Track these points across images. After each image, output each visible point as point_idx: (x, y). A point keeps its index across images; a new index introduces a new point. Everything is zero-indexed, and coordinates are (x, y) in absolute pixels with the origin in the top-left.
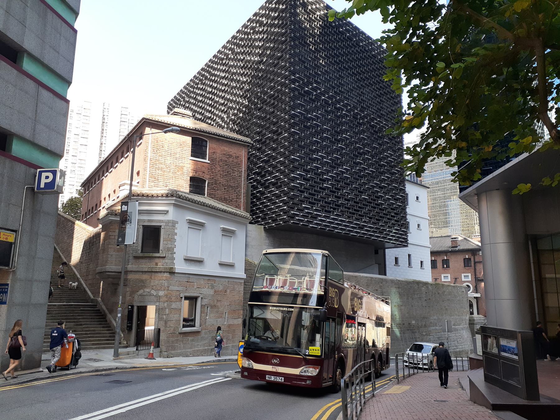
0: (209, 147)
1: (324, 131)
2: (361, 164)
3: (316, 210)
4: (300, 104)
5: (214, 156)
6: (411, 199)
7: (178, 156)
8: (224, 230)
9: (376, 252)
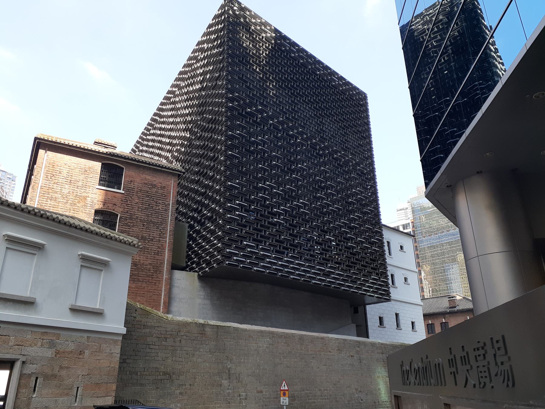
0: (127, 175)
1: (272, 158)
2: (323, 199)
3: (263, 249)
4: (239, 125)
5: (132, 185)
6: (395, 248)
7: (80, 184)
8: (84, 258)
9: (356, 311)
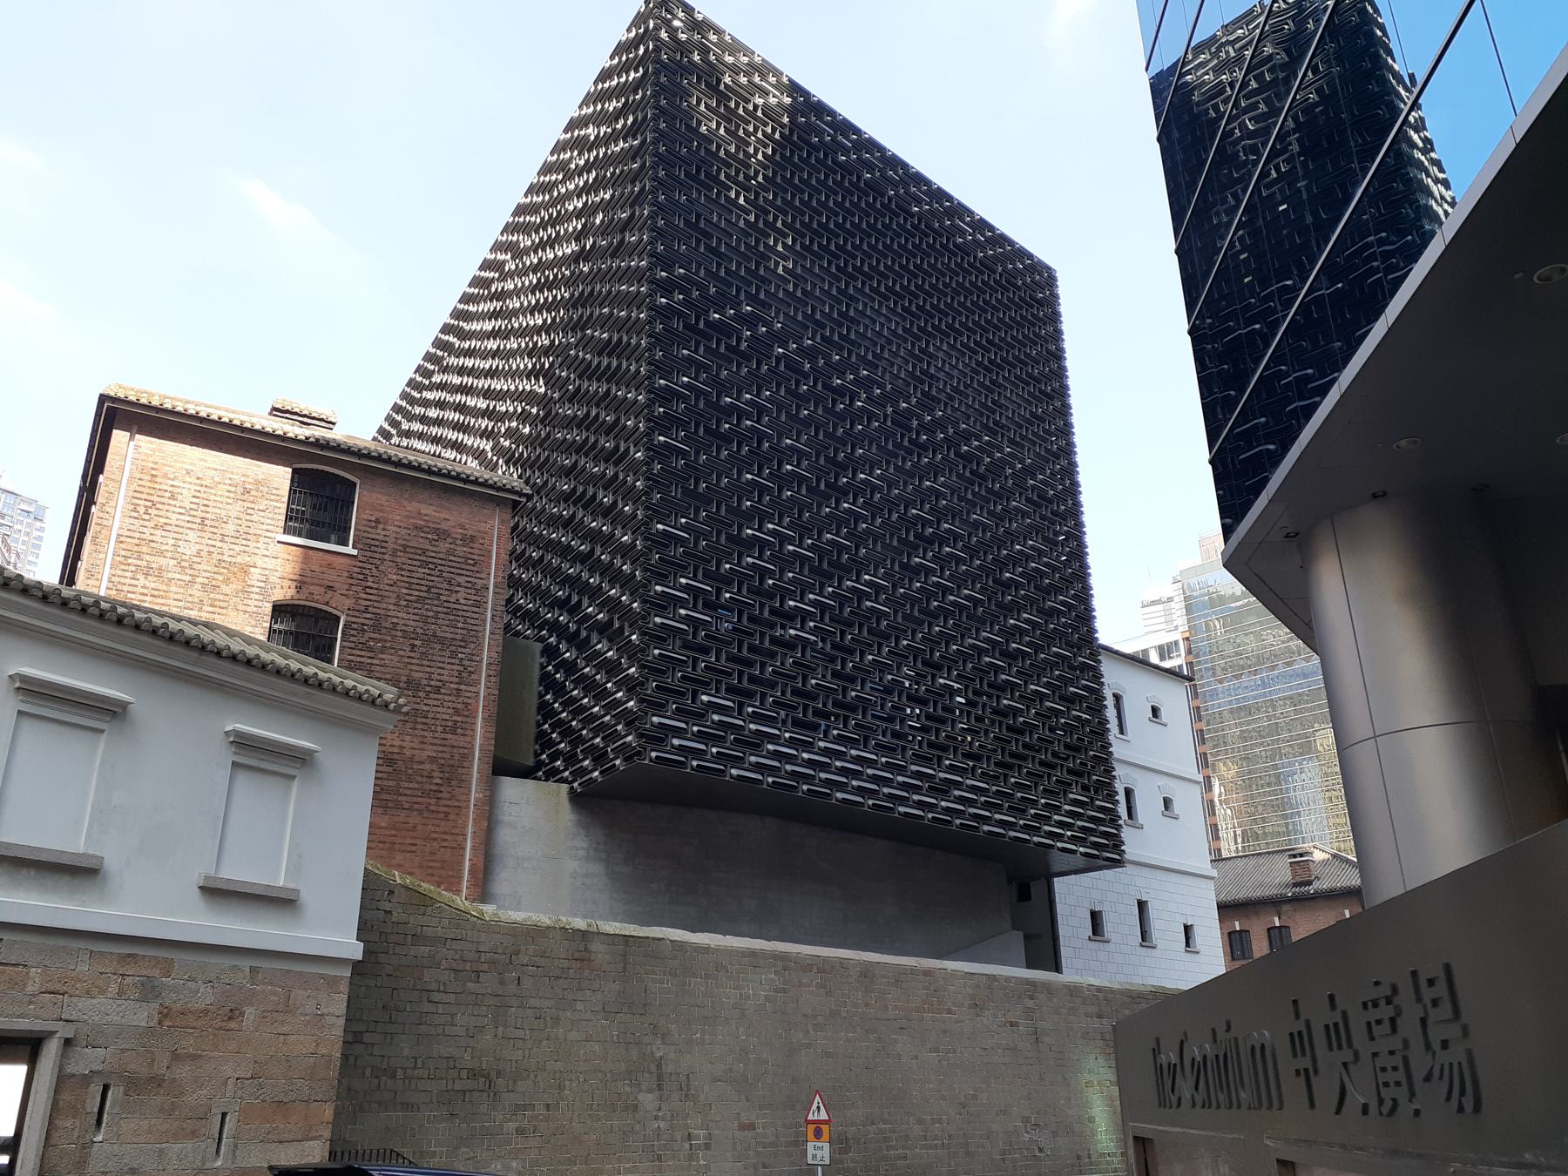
0: (365, 502)
1: (784, 455)
2: (929, 572)
3: (756, 717)
4: (689, 359)
5: (379, 533)
6: (1136, 712)
7: (230, 528)
8: (242, 743)
9: (1024, 895)
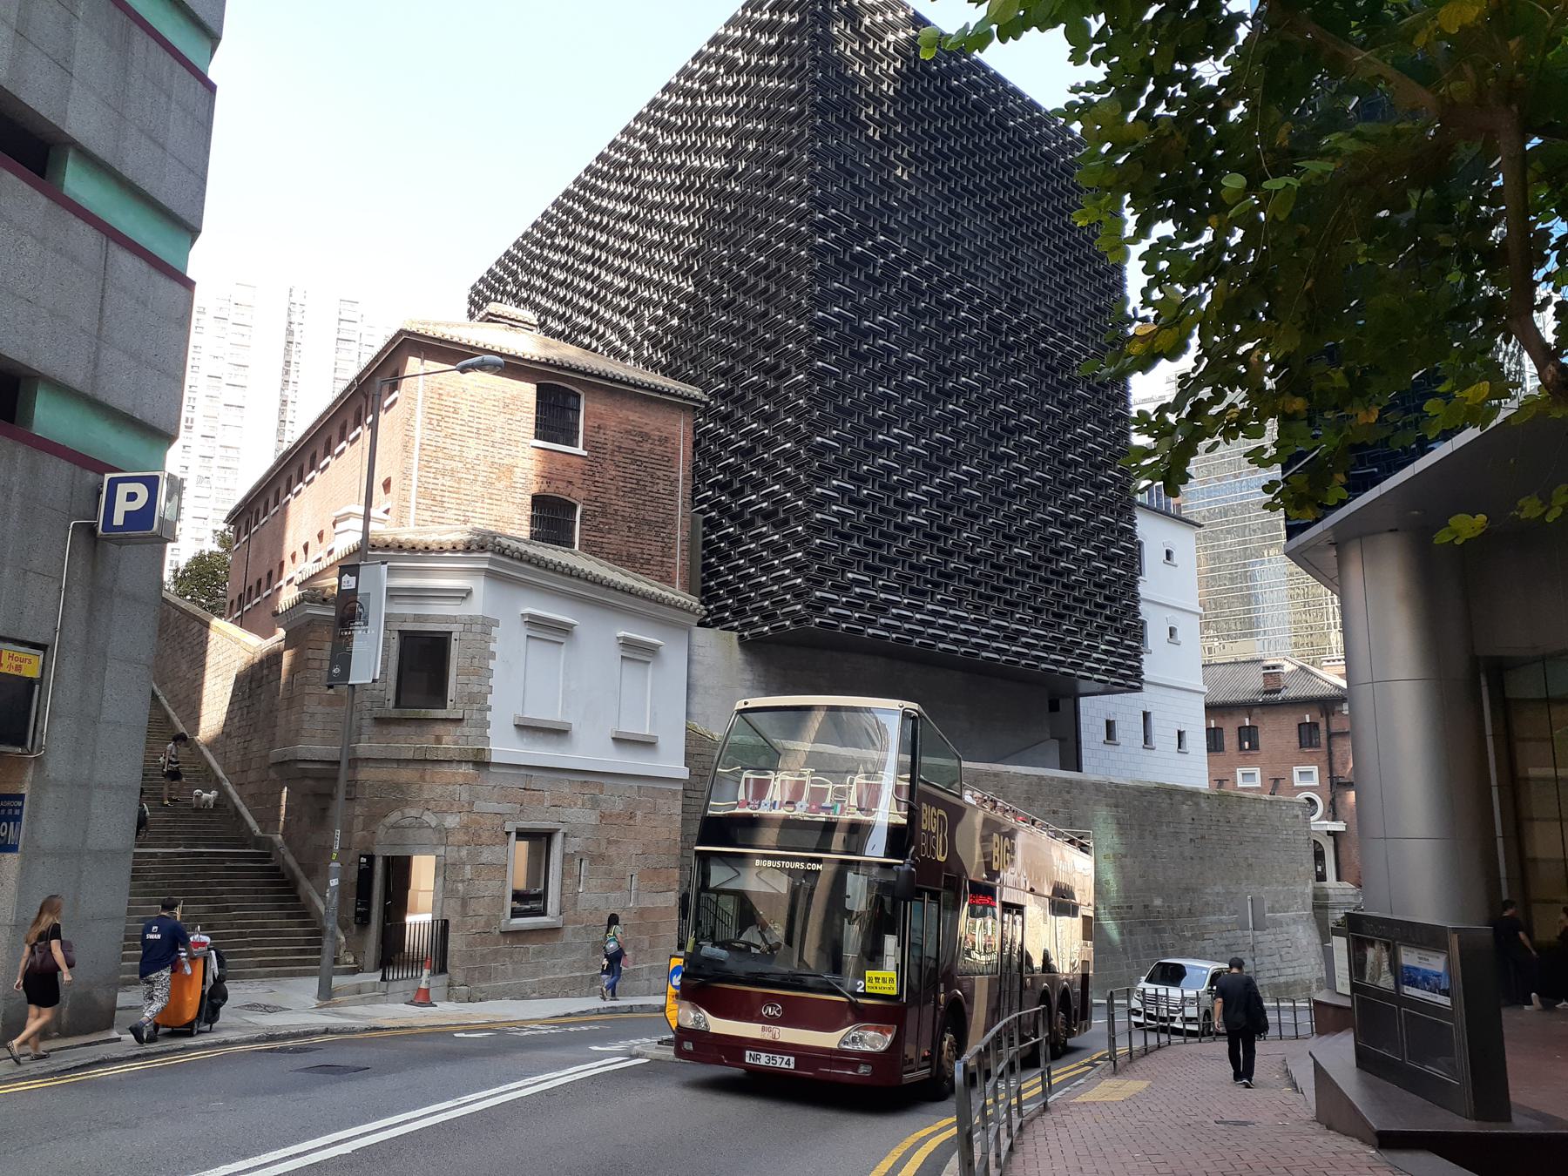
0: (587, 412)
1: (906, 367)
2: (1010, 458)
3: (885, 588)
4: (839, 291)
5: (601, 437)
6: (1151, 557)
7: (498, 435)
8: (627, 644)
9: (1054, 706)
